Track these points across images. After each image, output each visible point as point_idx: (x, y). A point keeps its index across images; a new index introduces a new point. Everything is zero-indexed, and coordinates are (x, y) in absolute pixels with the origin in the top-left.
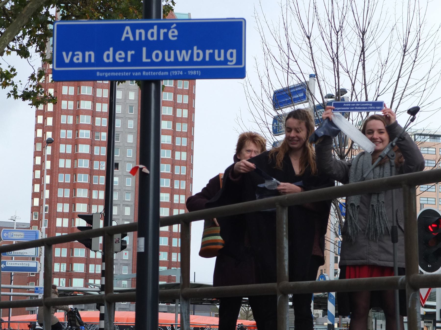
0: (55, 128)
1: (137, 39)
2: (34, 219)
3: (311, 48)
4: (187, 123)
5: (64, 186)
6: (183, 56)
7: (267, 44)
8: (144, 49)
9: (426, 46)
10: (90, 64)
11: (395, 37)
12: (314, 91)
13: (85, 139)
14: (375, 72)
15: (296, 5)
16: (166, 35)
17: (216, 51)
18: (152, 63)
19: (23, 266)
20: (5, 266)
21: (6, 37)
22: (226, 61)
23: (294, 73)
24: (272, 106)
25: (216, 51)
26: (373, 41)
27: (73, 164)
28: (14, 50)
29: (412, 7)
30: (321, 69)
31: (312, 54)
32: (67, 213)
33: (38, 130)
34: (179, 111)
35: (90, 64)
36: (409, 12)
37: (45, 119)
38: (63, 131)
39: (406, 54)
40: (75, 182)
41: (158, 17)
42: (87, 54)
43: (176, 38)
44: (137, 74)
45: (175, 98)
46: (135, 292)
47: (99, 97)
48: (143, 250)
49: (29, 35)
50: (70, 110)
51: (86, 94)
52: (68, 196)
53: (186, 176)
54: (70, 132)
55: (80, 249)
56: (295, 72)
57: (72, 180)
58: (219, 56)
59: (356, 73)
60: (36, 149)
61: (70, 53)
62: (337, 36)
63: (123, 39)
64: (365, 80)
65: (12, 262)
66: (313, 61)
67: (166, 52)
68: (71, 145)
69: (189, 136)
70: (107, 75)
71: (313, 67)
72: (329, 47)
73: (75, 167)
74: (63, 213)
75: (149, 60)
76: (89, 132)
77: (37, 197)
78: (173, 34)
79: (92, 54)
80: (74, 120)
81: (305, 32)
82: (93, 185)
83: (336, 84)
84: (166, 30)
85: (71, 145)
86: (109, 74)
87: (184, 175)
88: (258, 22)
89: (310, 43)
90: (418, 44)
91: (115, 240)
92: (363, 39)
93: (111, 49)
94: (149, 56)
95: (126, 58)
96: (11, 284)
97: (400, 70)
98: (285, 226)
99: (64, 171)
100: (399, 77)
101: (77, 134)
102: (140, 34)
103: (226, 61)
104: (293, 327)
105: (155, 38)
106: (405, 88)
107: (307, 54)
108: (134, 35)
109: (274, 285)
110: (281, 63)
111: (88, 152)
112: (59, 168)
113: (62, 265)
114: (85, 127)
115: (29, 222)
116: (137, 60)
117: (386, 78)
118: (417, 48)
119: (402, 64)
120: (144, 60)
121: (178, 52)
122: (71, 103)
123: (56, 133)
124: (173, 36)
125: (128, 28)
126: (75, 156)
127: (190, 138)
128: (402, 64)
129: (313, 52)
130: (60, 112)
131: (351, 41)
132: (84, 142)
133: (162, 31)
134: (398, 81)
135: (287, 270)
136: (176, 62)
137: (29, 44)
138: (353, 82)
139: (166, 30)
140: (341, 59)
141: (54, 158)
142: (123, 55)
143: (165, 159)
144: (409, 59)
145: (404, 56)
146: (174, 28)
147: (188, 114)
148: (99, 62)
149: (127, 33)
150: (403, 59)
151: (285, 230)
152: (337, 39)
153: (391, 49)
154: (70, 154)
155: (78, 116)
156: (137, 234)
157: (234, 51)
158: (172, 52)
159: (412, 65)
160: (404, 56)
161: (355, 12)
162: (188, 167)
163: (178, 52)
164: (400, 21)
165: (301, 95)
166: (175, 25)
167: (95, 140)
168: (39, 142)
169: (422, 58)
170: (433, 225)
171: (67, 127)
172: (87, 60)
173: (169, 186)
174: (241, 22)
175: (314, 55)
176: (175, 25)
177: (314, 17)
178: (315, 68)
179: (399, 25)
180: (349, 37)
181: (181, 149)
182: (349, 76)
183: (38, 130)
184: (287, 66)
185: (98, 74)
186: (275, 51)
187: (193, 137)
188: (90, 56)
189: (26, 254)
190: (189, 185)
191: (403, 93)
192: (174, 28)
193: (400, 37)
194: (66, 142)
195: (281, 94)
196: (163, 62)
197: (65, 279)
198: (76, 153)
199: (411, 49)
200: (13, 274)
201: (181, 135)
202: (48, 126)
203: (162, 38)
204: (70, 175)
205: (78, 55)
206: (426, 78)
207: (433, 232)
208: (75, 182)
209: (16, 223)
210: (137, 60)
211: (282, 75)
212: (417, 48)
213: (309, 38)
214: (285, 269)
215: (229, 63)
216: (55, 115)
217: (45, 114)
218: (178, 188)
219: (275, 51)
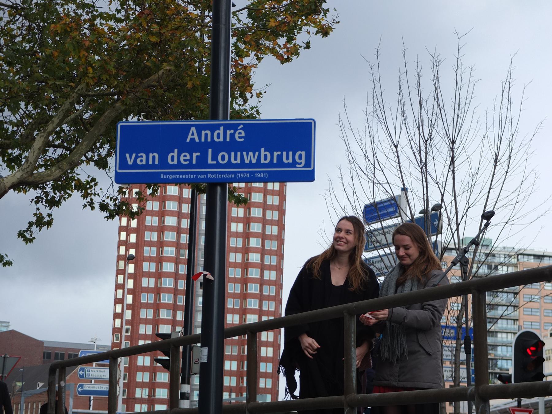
0: (139, 245)
1: (203, 140)
2: (115, 341)
3: (398, 157)
4: (277, 240)
5: (147, 306)
6: (250, 157)
7: (352, 153)
8: (210, 151)
9: (519, 157)
10: (154, 166)
11: (486, 146)
12: (400, 202)
13: (170, 257)
14: (465, 183)
15: (383, 113)
16: (233, 136)
17: (285, 153)
18: (218, 165)
19: (101, 389)
20: (82, 389)
21: (83, 146)
22: (294, 164)
23: (380, 184)
25: (285, 153)
26: (464, 150)
27: (156, 283)
28: (93, 161)
29: (504, 115)
30: (409, 179)
31: (399, 164)
32: (149, 335)
33: (121, 247)
34: (268, 228)
35: (154, 166)
36: (500, 121)
37: (128, 236)
38: (146, 249)
39: (498, 164)
40: (158, 302)
41: (225, 118)
42: (151, 155)
43: (243, 140)
44: (202, 177)
45: (264, 214)
47: (185, 213)
48: (206, 361)
49: (107, 144)
50: (155, 226)
51: (172, 209)
52: (151, 317)
53: (275, 296)
54: (154, 249)
55: (163, 373)
56: (381, 182)
57: (155, 300)
58: (288, 158)
59: (446, 184)
60: (118, 268)
61: (134, 155)
62: (426, 144)
63: (188, 140)
64: (455, 191)
65: (90, 386)
66: (401, 171)
67: (233, 154)
68: (155, 263)
69: (278, 254)
70: (171, 177)
71: (401, 177)
72: (418, 157)
73: (159, 286)
74: (146, 335)
75: (215, 162)
76: (174, 249)
77: (118, 318)
78: (240, 135)
79: (156, 155)
80: (159, 237)
81: (392, 141)
82: (178, 305)
83: (424, 195)
84: (232, 131)
85: (155, 263)
86: (173, 176)
87: (273, 296)
88: (343, 131)
89: (397, 152)
90: (511, 153)
91: (194, 361)
92: (452, 149)
93: (176, 151)
94: (215, 158)
95: (191, 160)
96: (89, 409)
97: (492, 181)
98: (353, 335)
99: (148, 290)
100: (490, 189)
101: (162, 251)
102: (206, 135)
103: (294, 164)
105: (221, 139)
106: (497, 200)
107: (394, 164)
108: (242, 156)
109: (342, 397)
110: (366, 173)
111: (173, 271)
112: (142, 288)
113: (144, 391)
114: (170, 244)
115: (110, 345)
116: (202, 162)
117: (476, 190)
118: (510, 158)
119: (494, 175)
120: (210, 162)
121: (245, 154)
122: (156, 219)
123: (139, 250)
124: (240, 138)
125: (193, 129)
126: (159, 275)
127: (280, 256)
128: (494, 175)
129: (401, 161)
130: (144, 228)
131: (440, 150)
132: (169, 260)
133: (229, 132)
134: (489, 192)
135: (355, 381)
136: (243, 164)
137: (109, 154)
138: (443, 193)
139: (232, 131)
140: (430, 168)
141: (137, 276)
142: (188, 157)
143: (253, 278)
144: (501, 169)
145: (495, 166)
146: (241, 129)
147: (278, 231)
148: (164, 163)
149: (193, 135)
150: (495, 170)
151: (353, 339)
152: (426, 148)
153: (482, 159)
154: (153, 272)
155: (163, 232)
157: (303, 153)
158: (239, 154)
159: (504, 176)
160: (495, 166)
161: (444, 120)
162: (277, 287)
163: (245, 154)
164: (492, 129)
165: (391, 210)
166: (242, 126)
167: (180, 257)
168: (122, 260)
169: (514, 169)
170: (532, 349)
171: (150, 244)
172: (151, 163)
173: (257, 307)
174: (311, 123)
175: (401, 165)
176: (242, 126)
177: (401, 124)
178: (402, 178)
180: (438, 146)
181: (270, 268)
182: (439, 188)
183: (121, 247)
184: (373, 176)
185: (162, 176)
186: (361, 161)
187: (283, 255)
188: (154, 157)
189: (104, 377)
190: (278, 306)
191: (495, 205)
192: (241, 129)
193: (491, 147)
194: (150, 259)
195: (370, 209)
196: (229, 165)
197: (147, 405)
198: (160, 271)
199: (503, 158)
200: (92, 398)
201: (270, 252)
202: (131, 243)
203: (228, 139)
204: (153, 295)
205: (142, 156)
206: (518, 190)
207: (532, 355)
208: (158, 302)
209: (97, 345)
210: (202, 162)
211: (367, 185)
212: (510, 158)
213: (396, 147)
214: (352, 380)
215: (297, 166)
216: (139, 231)
217: (128, 230)
218: (267, 309)
219: (361, 161)
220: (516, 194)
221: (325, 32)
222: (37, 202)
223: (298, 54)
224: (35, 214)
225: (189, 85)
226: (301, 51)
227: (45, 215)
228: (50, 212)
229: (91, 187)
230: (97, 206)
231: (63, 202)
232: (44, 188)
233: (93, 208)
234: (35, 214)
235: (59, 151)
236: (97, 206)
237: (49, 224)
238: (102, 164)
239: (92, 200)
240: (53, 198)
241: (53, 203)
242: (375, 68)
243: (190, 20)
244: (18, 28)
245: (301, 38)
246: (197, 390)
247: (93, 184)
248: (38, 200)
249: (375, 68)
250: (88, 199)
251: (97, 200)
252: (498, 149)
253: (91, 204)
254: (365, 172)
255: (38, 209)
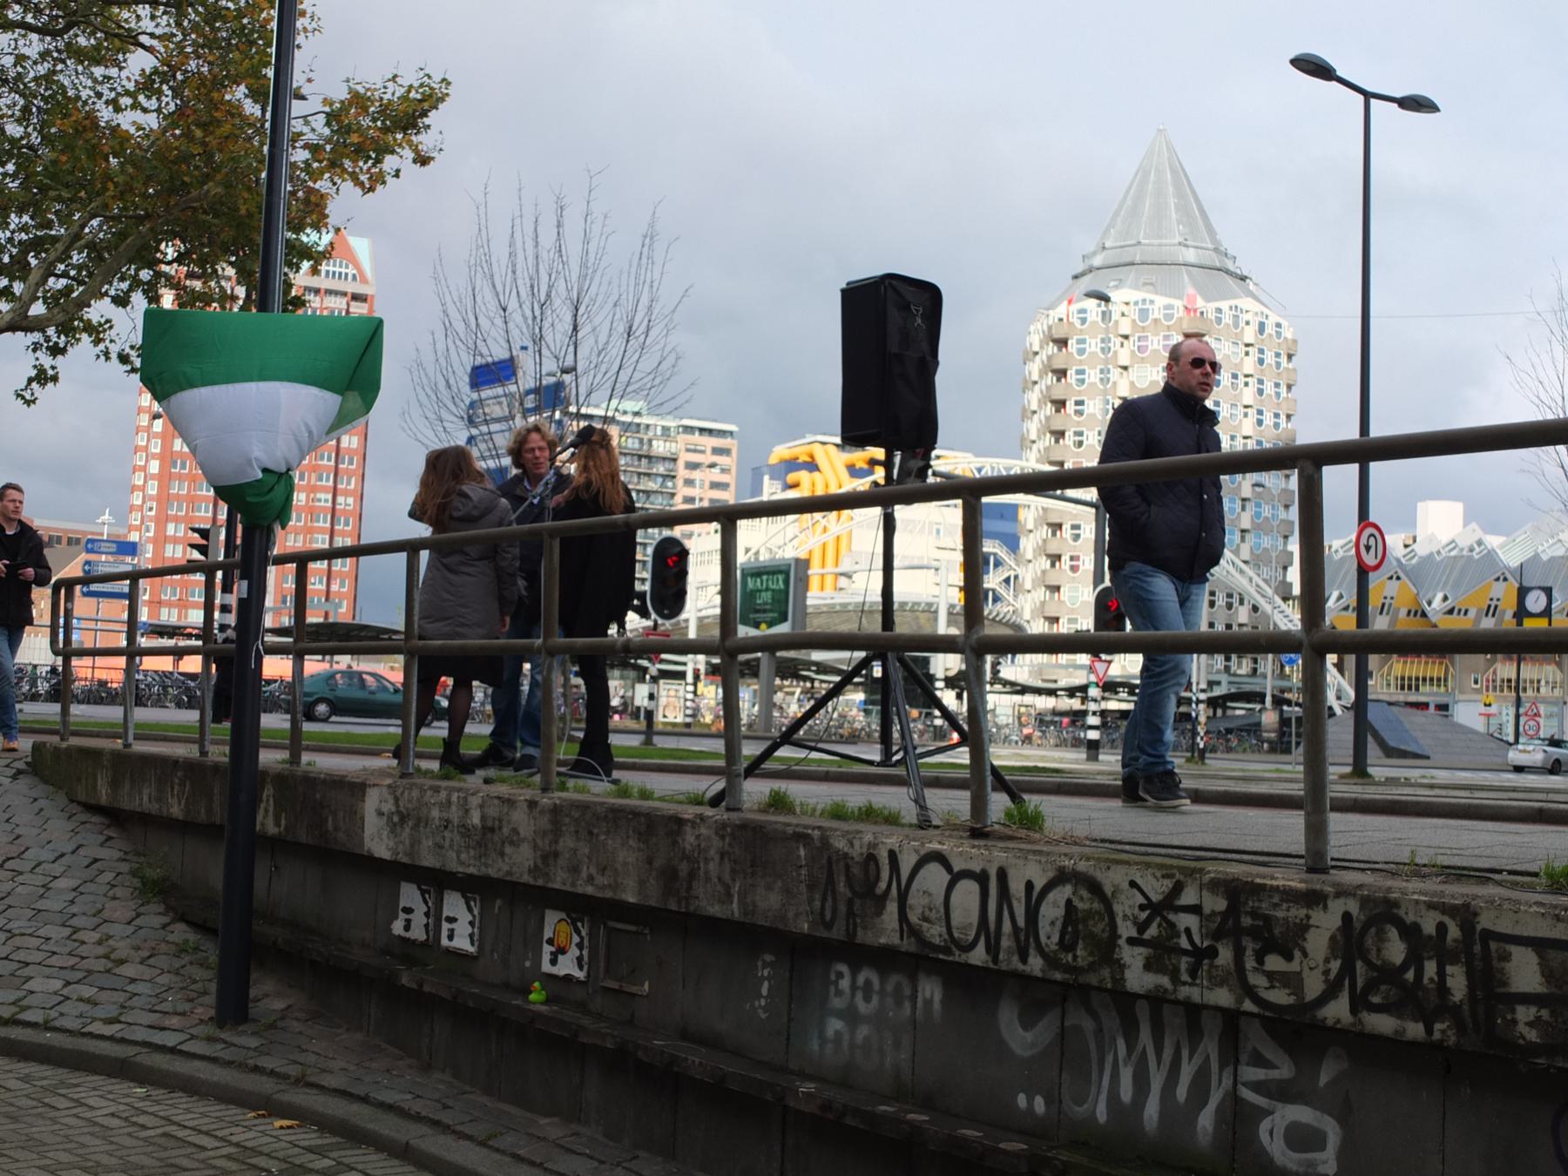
24: (467, 379)
46: (233, 646)
104: (84, 624)
145: (628, 341)
156: (191, 756)
160: (628, 341)
179: (623, 301)
186: (460, 326)
213: (504, 310)
219: (460, 326)
220: (652, 376)
221: (423, 160)
222: (34, 350)
223: (384, 183)
224: (35, 367)
225: (243, 212)
226: (388, 178)
227: (47, 366)
228: (53, 363)
229: (105, 331)
230: (114, 356)
231: (69, 348)
232: (44, 332)
233: (108, 358)
234: (35, 367)
235: (63, 282)
236: (114, 356)
237: (55, 379)
238: (122, 301)
239: (107, 348)
240: (56, 344)
241: (56, 351)
242: (482, 208)
243: (246, 121)
244: (8, 107)
245: (390, 162)
246: (198, 608)
247: (106, 326)
248: (36, 347)
249: (482, 208)
250: (102, 346)
251: (114, 350)
252: (633, 319)
253: (107, 354)
254: (499, 288)
255: (37, 359)
